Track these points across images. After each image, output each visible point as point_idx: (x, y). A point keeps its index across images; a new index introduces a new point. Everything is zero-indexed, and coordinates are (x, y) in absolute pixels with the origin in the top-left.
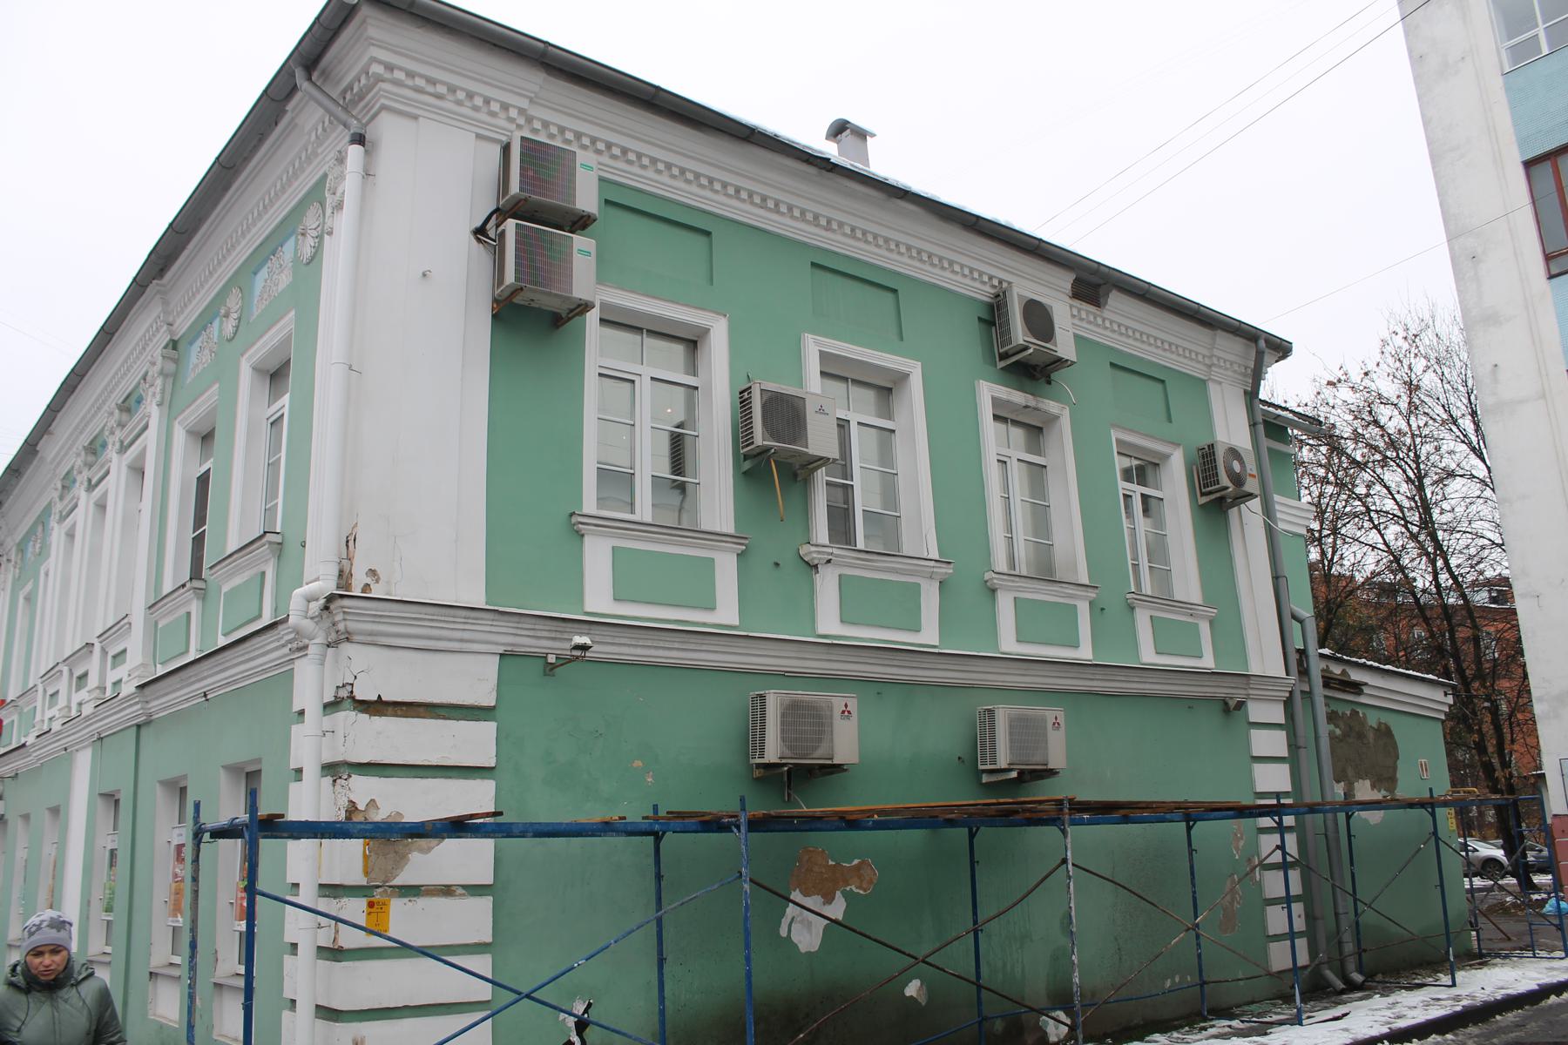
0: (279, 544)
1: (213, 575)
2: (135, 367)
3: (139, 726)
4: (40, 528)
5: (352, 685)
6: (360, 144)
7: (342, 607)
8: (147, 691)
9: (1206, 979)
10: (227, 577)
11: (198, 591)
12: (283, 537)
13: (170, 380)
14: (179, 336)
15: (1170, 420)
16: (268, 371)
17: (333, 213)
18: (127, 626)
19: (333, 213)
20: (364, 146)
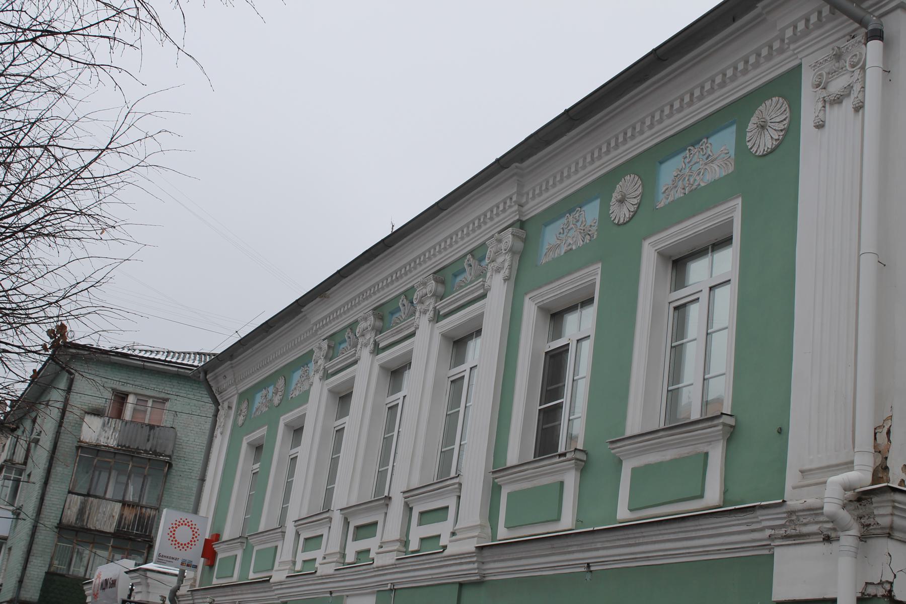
0: (731, 426)
1: (614, 449)
2: (461, 243)
3: (461, 585)
4: (281, 382)
5: (891, 583)
6: (880, 40)
7: (894, 501)
8: (486, 553)
9: (91, 493)
10: (635, 453)
11: (579, 462)
12: (736, 421)
13: (517, 257)
14: (527, 218)
15: (702, 291)
16: (670, 257)
17: (824, 107)
18: (456, 486)
19: (824, 107)
20: (882, 41)
